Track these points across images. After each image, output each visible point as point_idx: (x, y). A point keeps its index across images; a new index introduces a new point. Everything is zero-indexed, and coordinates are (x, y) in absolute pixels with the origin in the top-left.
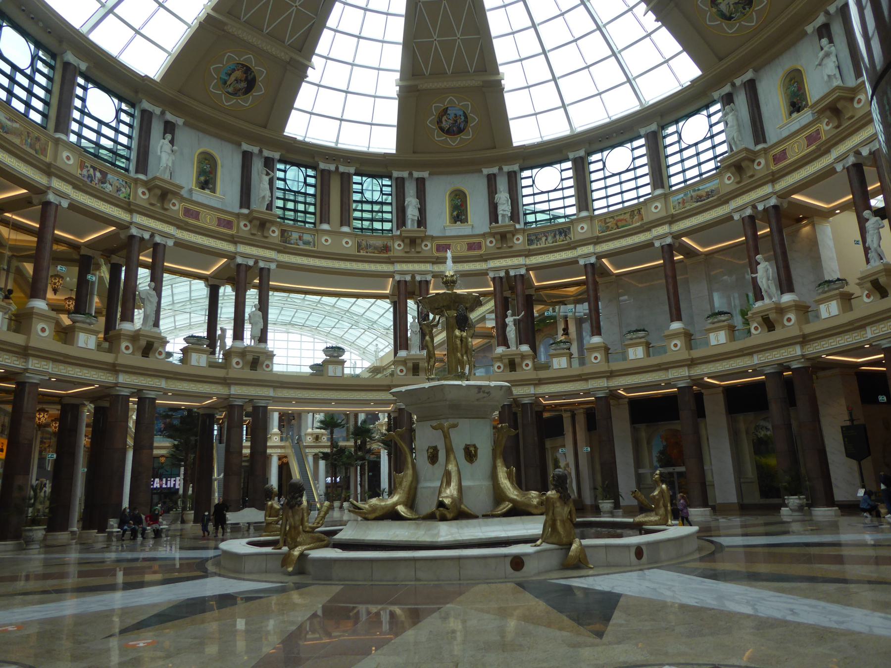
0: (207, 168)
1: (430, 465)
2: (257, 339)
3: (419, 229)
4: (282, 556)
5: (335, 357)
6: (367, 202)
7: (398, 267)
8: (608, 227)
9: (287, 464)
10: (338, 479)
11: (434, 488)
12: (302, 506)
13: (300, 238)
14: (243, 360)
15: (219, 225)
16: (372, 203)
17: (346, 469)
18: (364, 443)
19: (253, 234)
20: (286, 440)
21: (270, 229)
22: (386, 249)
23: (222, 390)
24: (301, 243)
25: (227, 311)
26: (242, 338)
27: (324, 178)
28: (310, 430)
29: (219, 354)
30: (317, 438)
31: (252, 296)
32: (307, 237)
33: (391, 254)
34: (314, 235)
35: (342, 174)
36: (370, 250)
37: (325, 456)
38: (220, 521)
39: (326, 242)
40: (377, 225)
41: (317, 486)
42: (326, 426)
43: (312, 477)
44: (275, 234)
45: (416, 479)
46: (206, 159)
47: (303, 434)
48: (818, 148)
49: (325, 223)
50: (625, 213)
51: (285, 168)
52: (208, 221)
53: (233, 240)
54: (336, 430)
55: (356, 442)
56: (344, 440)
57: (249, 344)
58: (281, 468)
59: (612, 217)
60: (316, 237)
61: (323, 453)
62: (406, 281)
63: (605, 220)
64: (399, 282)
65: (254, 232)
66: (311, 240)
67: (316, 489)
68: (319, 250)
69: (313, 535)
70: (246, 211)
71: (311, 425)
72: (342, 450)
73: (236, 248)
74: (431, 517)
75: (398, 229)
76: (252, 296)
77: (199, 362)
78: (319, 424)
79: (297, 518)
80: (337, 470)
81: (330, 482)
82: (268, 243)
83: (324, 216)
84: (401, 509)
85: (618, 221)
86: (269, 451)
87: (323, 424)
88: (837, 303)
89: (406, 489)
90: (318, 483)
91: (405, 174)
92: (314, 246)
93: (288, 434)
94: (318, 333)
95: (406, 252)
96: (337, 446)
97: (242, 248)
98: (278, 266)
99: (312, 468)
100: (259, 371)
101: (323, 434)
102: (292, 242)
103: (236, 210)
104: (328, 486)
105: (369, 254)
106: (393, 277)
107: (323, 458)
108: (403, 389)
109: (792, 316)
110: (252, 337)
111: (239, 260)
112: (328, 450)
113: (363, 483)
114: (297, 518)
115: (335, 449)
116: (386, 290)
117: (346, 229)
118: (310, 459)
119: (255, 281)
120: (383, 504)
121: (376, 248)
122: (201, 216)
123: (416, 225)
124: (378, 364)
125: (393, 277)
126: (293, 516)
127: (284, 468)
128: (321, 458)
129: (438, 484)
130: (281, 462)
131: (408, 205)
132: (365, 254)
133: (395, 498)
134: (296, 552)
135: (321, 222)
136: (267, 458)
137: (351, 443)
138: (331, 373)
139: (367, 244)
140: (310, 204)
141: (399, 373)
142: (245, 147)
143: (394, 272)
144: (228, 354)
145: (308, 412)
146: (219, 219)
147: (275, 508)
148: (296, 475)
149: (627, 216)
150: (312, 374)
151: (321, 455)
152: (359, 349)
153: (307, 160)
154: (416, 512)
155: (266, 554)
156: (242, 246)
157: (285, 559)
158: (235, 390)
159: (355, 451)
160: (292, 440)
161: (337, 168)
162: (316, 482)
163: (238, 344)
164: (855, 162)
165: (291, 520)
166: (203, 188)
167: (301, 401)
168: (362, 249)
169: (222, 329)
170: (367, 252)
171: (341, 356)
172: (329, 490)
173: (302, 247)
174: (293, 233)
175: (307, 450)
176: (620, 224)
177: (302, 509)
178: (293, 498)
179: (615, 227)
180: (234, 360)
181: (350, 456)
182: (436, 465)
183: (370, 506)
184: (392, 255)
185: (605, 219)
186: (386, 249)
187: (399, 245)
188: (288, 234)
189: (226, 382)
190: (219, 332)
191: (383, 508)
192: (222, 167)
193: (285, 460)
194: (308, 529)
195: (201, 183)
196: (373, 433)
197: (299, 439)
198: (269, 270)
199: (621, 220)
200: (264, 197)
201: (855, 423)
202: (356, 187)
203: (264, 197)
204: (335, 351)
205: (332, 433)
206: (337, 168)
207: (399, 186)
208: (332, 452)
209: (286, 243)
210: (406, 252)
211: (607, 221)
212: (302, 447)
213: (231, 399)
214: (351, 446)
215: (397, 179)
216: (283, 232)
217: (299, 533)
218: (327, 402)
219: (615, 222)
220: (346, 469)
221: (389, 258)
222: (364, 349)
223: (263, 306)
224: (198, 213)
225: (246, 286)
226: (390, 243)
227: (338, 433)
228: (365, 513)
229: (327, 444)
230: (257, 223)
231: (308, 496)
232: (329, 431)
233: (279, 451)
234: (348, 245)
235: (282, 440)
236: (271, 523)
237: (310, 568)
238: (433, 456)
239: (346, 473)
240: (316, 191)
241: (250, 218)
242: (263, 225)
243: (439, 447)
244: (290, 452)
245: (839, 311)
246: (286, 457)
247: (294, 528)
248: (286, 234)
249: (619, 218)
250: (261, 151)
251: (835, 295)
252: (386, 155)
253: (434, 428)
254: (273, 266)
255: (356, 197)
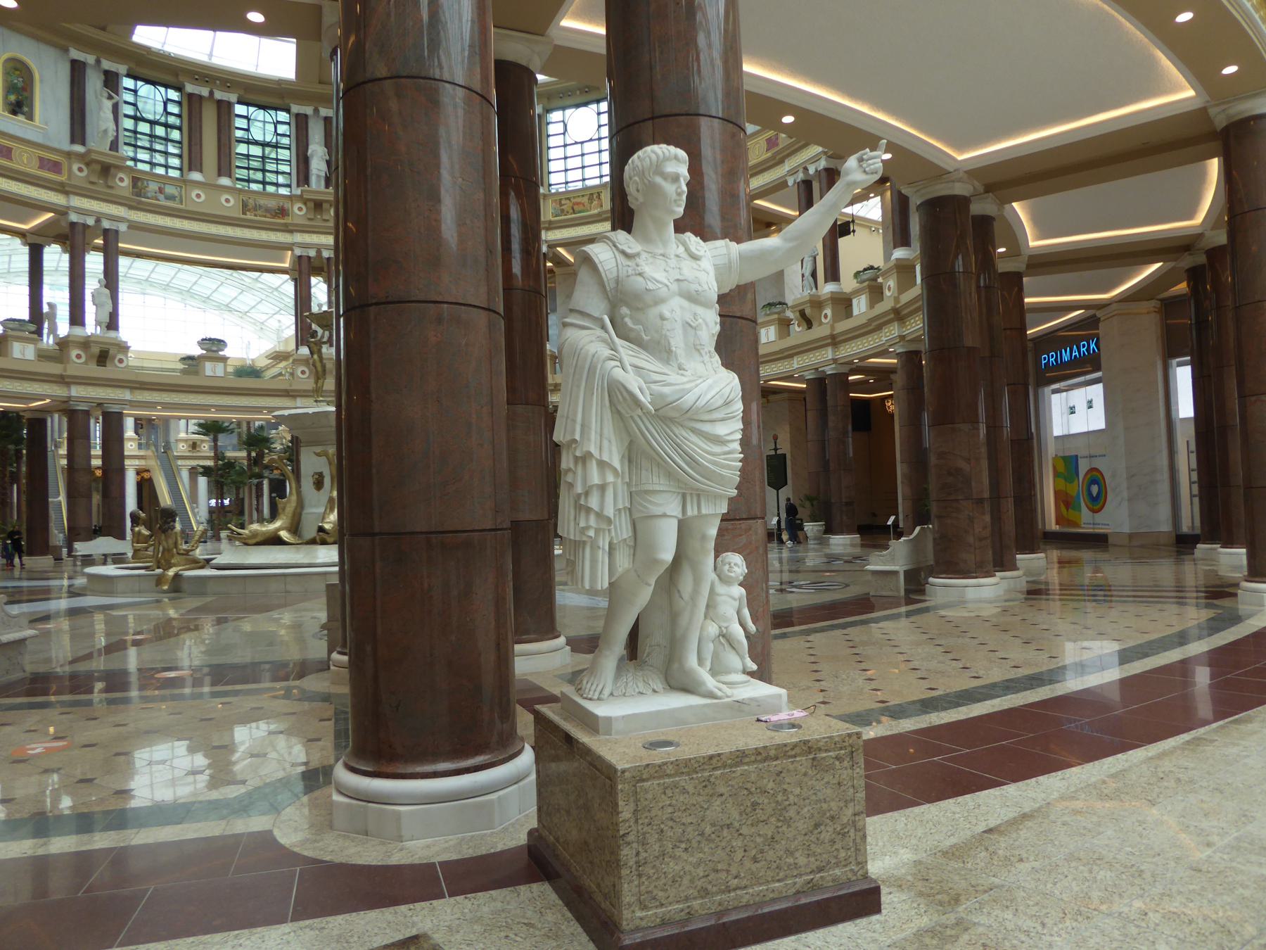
0: (19, 82)
1: (315, 491)
2: (104, 325)
3: (327, 190)
4: (156, 577)
5: (214, 351)
6: (256, 143)
7: (299, 238)
8: (562, 211)
9: (150, 480)
10: (227, 502)
11: (319, 513)
12: (175, 530)
13: (161, 190)
14: (86, 352)
15: (41, 167)
16: (264, 145)
17: (238, 489)
18: (261, 456)
19: (92, 183)
20: (147, 446)
21: (116, 176)
22: (282, 212)
23: (59, 391)
24: (161, 197)
25: (56, 293)
26: (82, 324)
27: (192, 104)
28: (182, 435)
29: (48, 337)
30: (194, 446)
31: (94, 263)
32: (170, 190)
33: (288, 220)
34: (181, 187)
35: (219, 102)
36: (259, 212)
37: (207, 471)
38: (169, 515)
39: (198, 198)
40: (271, 189)
41: (196, 510)
42: (207, 431)
43: (187, 498)
44: (123, 183)
45: (301, 504)
46: (16, 69)
47: (172, 439)
48: (773, 157)
49: (196, 170)
50: (583, 196)
51: (136, 85)
52: (25, 161)
53: (62, 189)
54: (221, 436)
55: (249, 455)
56: (234, 449)
57: (94, 332)
58: (140, 485)
59: (569, 199)
60: (183, 189)
61: (203, 467)
62: (309, 258)
63: (560, 202)
64: (300, 257)
65: (94, 179)
66: (176, 194)
67: (195, 515)
68: (188, 208)
69: (188, 557)
70: (79, 148)
71: (184, 431)
72: (230, 465)
73: (68, 201)
74: (313, 542)
75: (298, 185)
76: (94, 263)
77: (24, 354)
78: (196, 427)
79: (171, 542)
80: (225, 491)
81: (214, 505)
82: (112, 195)
83: (193, 160)
84: (284, 534)
85: (574, 204)
86: (127, 462)
87: (203, 428)
88: (775, 328)
89: (290, 515)
90: (197, 507)
91: (308, 110)
92: (181, 202)
93: (148, 439)
94: (191, 297)
95: (310, 219)
96: (223, 458)
97: (77, 202)
98: (129, 227)
99: (187, 486)
100: (109, 368)
101: (202, 441)
102: (149, 195)
103: (65, 145)
104: (211, 511)
105: (258, 218)
106: (292, 250)
107: (203, 474)
108: (286, 413)
109: (828, 311)
110: (98, 323)
111: (74, 217)
112: (210, 463)
113: (260, 507)
114: (171, 542)
115: (220, 462)
116: (284, 262)
117: (225, 181)
118: (185, 474)
119: (96, 241)
120: (264, 529)
121: (267, 210)
122: (15, 154)
123: (323, 183)
124: (281, 348)
125: (292, 250)
126: (166, 540)
127: (146, 487)
128: (201, 473)
129: (322, 510)
130: (139, 477)
131: (312, 156)
132: (253, 217)
133: (278, 524)
134: (171, 572)
135: (190, 169)
136: (121, 471)
137: (244, 454)
138: (208, 372)
139: (256, 205)
140: (173, 127)
141: (300, 375)
142: (75, 54)
143: (293, 244)
144: (63, 344)
145: (180, 418)
146: (41, 159)
147: (144, 535)
148: (165, 499)
149: (585, 200)
150: (183, 372)
151: (201, 470)
152: (255, 324)
153: (169, 78)
154: (299, 536)
155: (139, 576)
156: (77, 198)
157: (159, 580)
158: (76, 391)
159: (249, 466)
160: (156, 446)
161: (211, 93)
162: (195, 505)
163: (78, 331)
164: (804, 179)
165: (164, 543)
166: (14, 113)
167: (167, 406)
168: (249, 210)
169: (49, 304)
170: (256, 215)
171: (223, 350)
172: (214, 516)
173: (163, 202)
174: (150, 182)
175: (180, 462)
176: (576, 208)
177: (176, 533)
178: (166, 522)
179: (571, 211)
180: (74, 353)
181: (242, 473)
182: (322, 491)
183: (250, 531)
184: (290, 221)
185: (561, 200)
186: (282, 212)
187: (300, 209)
188: (143, 184)
189: (63, 380)
190: (46, 309)
191: (264, 533)
192: (41, 81)
193: (146, 475)
194: (182, 552)
195: (11, 104)
196: (273, 443)
197: (168, 447)
198: (117, 232)
199: (578, 204)
200: (105, 131)
201: (779, 452)
202: (240, 123)
203: (105, 131)
204: (213, 343)
205: (215, 440)
206: (211, 93)
207: (301, 123)
208: (216, 465)
209: (140, 196)
210: (310, 219)
211: (563, 202)
212: (171, 458)
213: (72, 403)
214: (243, 458)
215: (297, 115)
216: (135, 181)
217: (173, 556)
218: (205, 408)
219: (571, 205)
220: (238, 489)
221: (286, 225)
222: (262, 323)
223: (111, 278)
224: (9, 150)
225: (84, 246)
226: (287, 205)
227: (223, 439)
228: (245, 539)
229: (208, 454)
230: (98, 167)
231: (182, 522)
232: (212, 436)
233: (137, 462)
234: (229, 204)
235: (140, 446)
236: (139, 550)
237: (185, 586)
238: (319, 482)
239: (238, 494)
240: (182, 162)
241: (87, 160)
242: (106, 170)
243: (324, 474)
244: (153, 464)
245: (776, 338)
246: (148, 471)
247: (167, 551)
248: (139, 184)
249: (578, 200)
250: (98, 62)
251: (774, 320)
252: (280, 82)
253: (318, 455)
254: (123, 227)
255: (239, 134)
